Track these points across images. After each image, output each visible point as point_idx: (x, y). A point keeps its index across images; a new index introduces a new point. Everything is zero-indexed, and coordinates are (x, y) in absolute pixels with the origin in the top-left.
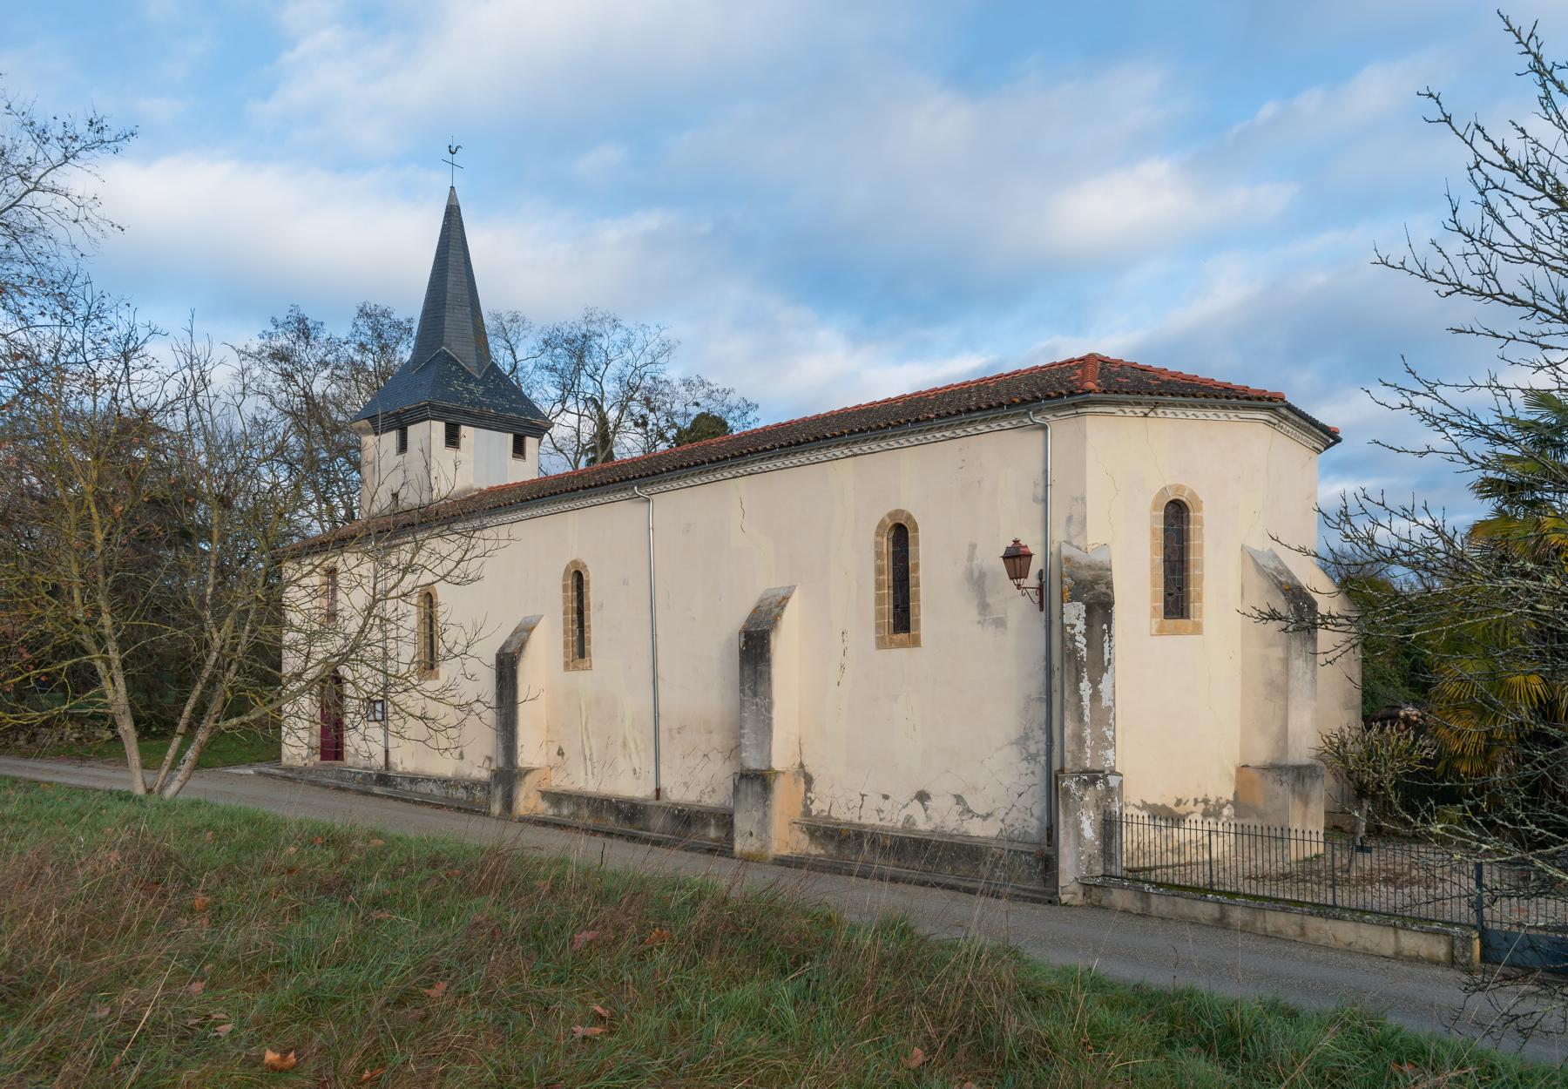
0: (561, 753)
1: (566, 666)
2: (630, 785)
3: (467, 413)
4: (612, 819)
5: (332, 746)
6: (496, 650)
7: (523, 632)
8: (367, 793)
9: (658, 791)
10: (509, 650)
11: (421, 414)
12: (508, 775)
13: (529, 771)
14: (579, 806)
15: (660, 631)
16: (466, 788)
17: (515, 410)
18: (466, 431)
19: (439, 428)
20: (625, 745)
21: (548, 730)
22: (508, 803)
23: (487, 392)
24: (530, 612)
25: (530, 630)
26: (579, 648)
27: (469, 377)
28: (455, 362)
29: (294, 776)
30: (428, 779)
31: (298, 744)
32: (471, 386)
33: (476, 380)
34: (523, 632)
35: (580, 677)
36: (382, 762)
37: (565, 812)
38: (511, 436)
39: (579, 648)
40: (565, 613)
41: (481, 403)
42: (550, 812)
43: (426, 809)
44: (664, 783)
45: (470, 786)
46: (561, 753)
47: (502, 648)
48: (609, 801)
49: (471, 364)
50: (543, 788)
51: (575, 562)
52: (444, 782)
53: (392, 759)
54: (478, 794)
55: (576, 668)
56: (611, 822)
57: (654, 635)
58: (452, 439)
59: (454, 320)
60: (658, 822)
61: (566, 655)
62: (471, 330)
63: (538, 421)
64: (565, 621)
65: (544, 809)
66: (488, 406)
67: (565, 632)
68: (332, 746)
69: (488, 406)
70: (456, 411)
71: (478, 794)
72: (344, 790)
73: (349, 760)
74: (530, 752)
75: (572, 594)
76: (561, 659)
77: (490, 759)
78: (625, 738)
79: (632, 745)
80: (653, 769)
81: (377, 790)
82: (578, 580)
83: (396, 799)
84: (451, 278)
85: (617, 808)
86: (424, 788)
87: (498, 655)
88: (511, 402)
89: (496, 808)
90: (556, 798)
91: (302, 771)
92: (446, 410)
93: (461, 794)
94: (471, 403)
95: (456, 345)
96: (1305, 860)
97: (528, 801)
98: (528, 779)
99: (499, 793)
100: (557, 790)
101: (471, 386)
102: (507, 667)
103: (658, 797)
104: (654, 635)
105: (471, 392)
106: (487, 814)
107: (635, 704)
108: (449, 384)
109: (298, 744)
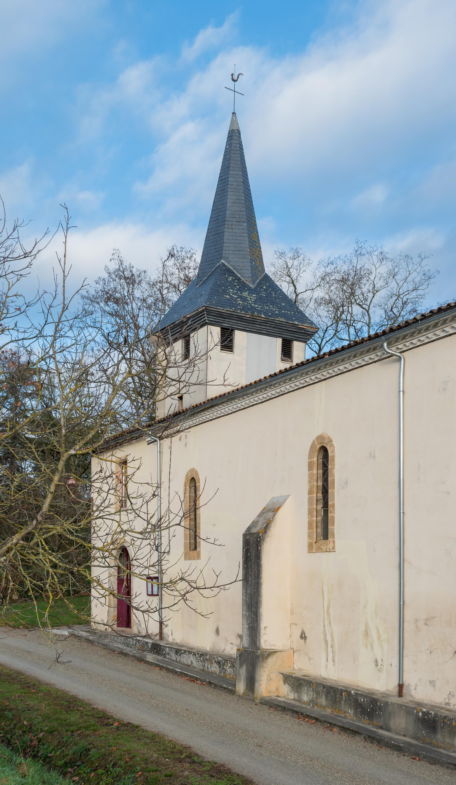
0: (303, 637)
1: (310, 546)
2: (376, 681)
3: (240, 318)
4: (351, 711)
5: (124, 615)
6: (243, 531)
7: (270, 512)
8: (141, 660)
9: (401, 686)
10: (254, 530)
11: (199, 320)
12: (252, 656)
13: (271, 653)
14: (318, 693)
15: (408, 509)
16: (219, 663)
17: (284, 316)
18: (240, 337)
19: (216, 331)
20: (367, 633)
21: (292, 613)
22: (251, 682)
23: (259, 300)
24: (277, 494)
25: (275, 510)
26: (323, 529)
27: (243, 286)
28: (231, 273)
29: (96, 641)
30: (190, 651)
31: (102, 611)
32: (245, 294)
33: (250, 289)
34: (270, 512)
35: (323, 558)
36: (157, 631)
37: (305, 698)
38: (280, 341)
39: (323, 529)
40: (310, 492)
41: (253, 309)
42: (292, 696)
43: (183, 679)
44: (408, 679)
45: (223, 661)
46: (303, 637)
47: (249, 529)
48: (349, 693)
49: (245, 275)
50: (287, 671)
51: (320, 438)
52: (202, 655)
53: (165, 630)
54: (229, 670)
55: (319, 550)
56: (349, 715)
57: (401, 514)
58: (227, 344)
59: (233, 235)
60: (400, 722)
61: (310, 536)
62: (246, 244)
63: (305, 326)
64: (310, 500)
65: (285, 693)
66: (260, 312)
67: (310, 512)
68: (124, 615)
69: (260, 312)
70: (230, 316)
71: (229, 670)
72: (126, 655)
73: (134, 629)
74: (272, 635)
75: (317, 472)
76: (305, 541)
77: (240, 637)
78: (367, 626)
79: (373, 633)
80: (395, 662)
81: (150, 657)
82: (324, 454)
83: (161, 668)
84: (231, 197)
85: (356, 700)
86: (187, 659)
87: (244, 535)
88: (280, 309)
89: (241, 687)
90: (297, 682)
91: (104, 635)
92: (220, 315)
93: (215, 668)
94: (244, 308)
95: (232, 260)
96: (91, 539)
97: (270, 684)
98: (271, 660)
99: (243, 672)
100: (298, 674)
101: (245, 294)
102: (253, 547)
103: (400, 694)
104: (401, 514)
105: (244, 299)
106: (232, 692)
107: (379, 590)
108: (225, 292)
109: (102, 611)
